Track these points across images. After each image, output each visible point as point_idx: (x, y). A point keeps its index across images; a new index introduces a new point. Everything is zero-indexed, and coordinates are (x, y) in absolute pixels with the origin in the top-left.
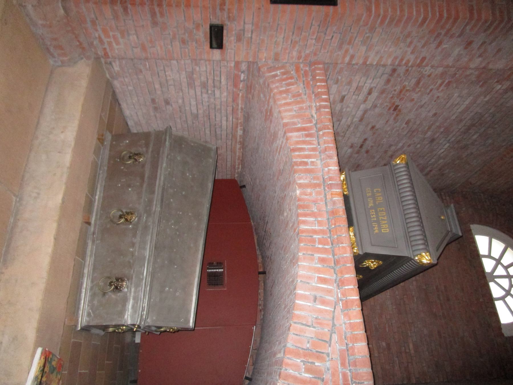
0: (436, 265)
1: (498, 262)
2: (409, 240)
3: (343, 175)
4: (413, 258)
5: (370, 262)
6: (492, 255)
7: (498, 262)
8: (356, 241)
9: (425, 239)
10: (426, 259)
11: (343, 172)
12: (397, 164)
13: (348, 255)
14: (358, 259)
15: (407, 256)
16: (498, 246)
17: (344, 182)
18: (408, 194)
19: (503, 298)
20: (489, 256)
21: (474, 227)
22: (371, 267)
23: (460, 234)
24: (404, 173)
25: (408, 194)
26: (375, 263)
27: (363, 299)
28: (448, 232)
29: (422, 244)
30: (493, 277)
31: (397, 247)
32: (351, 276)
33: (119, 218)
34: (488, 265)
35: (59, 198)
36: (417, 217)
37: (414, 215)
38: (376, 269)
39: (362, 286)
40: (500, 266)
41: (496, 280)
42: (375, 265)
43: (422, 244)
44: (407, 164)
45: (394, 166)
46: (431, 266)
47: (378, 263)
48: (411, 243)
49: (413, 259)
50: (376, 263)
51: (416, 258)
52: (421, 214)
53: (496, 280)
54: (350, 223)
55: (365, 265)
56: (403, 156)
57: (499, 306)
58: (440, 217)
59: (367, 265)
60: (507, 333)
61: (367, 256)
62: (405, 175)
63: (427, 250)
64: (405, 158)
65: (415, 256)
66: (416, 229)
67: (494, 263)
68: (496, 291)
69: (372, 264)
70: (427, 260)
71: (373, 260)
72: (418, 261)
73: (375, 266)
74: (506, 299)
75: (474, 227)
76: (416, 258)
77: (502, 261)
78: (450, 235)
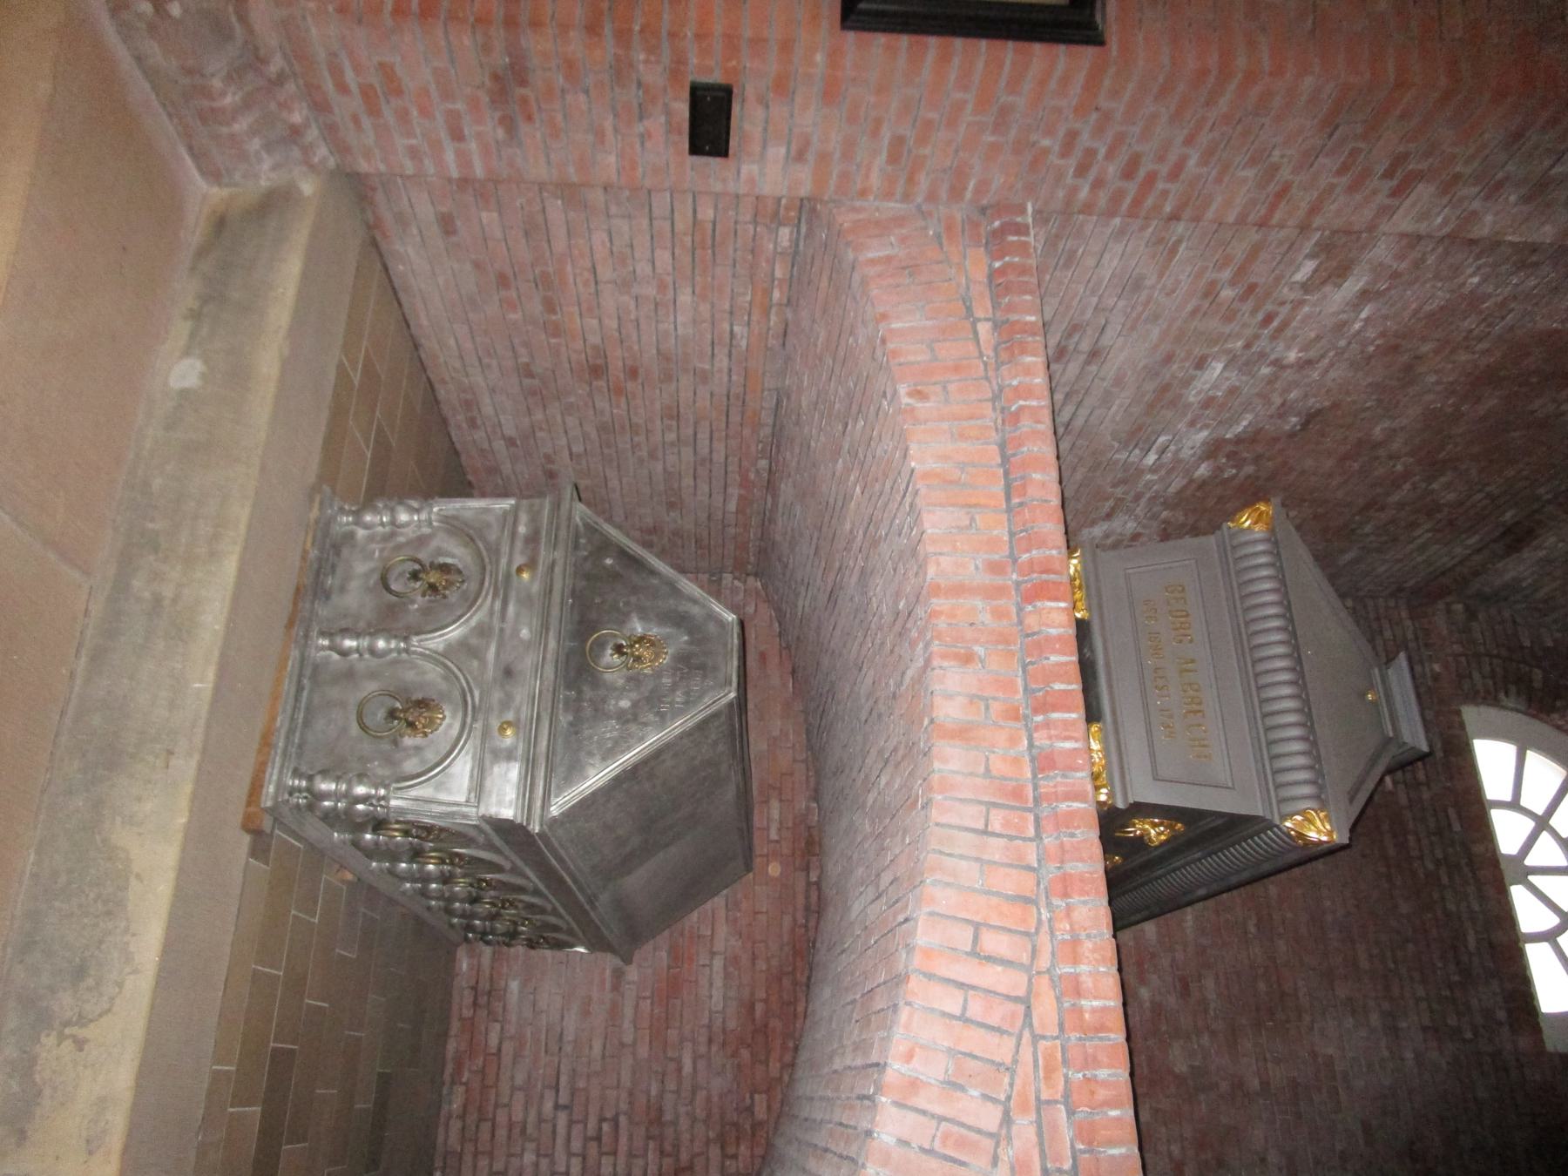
0: (1343, 848)
1: (1542, 823)
2: (1268, 767)
3: (1075, 558)
4: (1277, 822)
5: (1148, 823)
6: (1525, 802)
7: (1542, 823)
8: (1108, 766)
9: (1298, 668)
10: (1320, 832)
11: (1076, 551)
12: (1243, 530)
13: (1084, 809)
14: (1111, 822)
15: (1261, 814)
16: (1543, 774)
17: (1077, 582)
18: (1272, 611)
19: (1550, 937)
20: (1514, 805)
21: (1471, 714)
22: (1150, 839)
23: (1425, 748)
24: (1267, 586)
25: (1272, 611)
26: (1162, 828)
27: (1119, 923)
28: (1387, 741)
29: (1296, 711)
30: (1523, 874)
31: (1230, 785)
32: (1090, 864)
33: (386, 719)
34: (1509, 832)
35: (184, 820)
36: (1293, 670)
37: (1292, 718)
38: (1162, 844)
39: (1116, 883)
40: (1545, 836)
41: (1531, 878)
42: (1159, 834)
43: (1296, 711)
44: (1272, 531)
45: (1233, 536)
46: (1331, 851)
47: (1171, 827)
48: (1253, 666)
49: (1277, 827)
50: (1166, 827)
51: (1288, 824)
52: (1296, 623)
53: (1531, 878)
54: (1092, 714)
55: (1131, 832)
56: (1263, 508)
57: (1539, 959)
58: (1364, 695)
59: (1138, 832)
60: (1554, 1042)
61: (1140, 810)
62: (1305, 782)
63: (1321, 801)
64: (1267, 513)
65: (1284, 817)
66: (1294, 750)
67: (1530, 825)
68: (1529, 914)
69: (1155, 832)
70: (1319, 832)
71: (1156, 820)
72: (1293, 833)
73: (1163, 837)
74: (1507, 796)
75: (1470, 714)
76: (1288, 824)
77: (1553, 822)
78: (1393, 750)
